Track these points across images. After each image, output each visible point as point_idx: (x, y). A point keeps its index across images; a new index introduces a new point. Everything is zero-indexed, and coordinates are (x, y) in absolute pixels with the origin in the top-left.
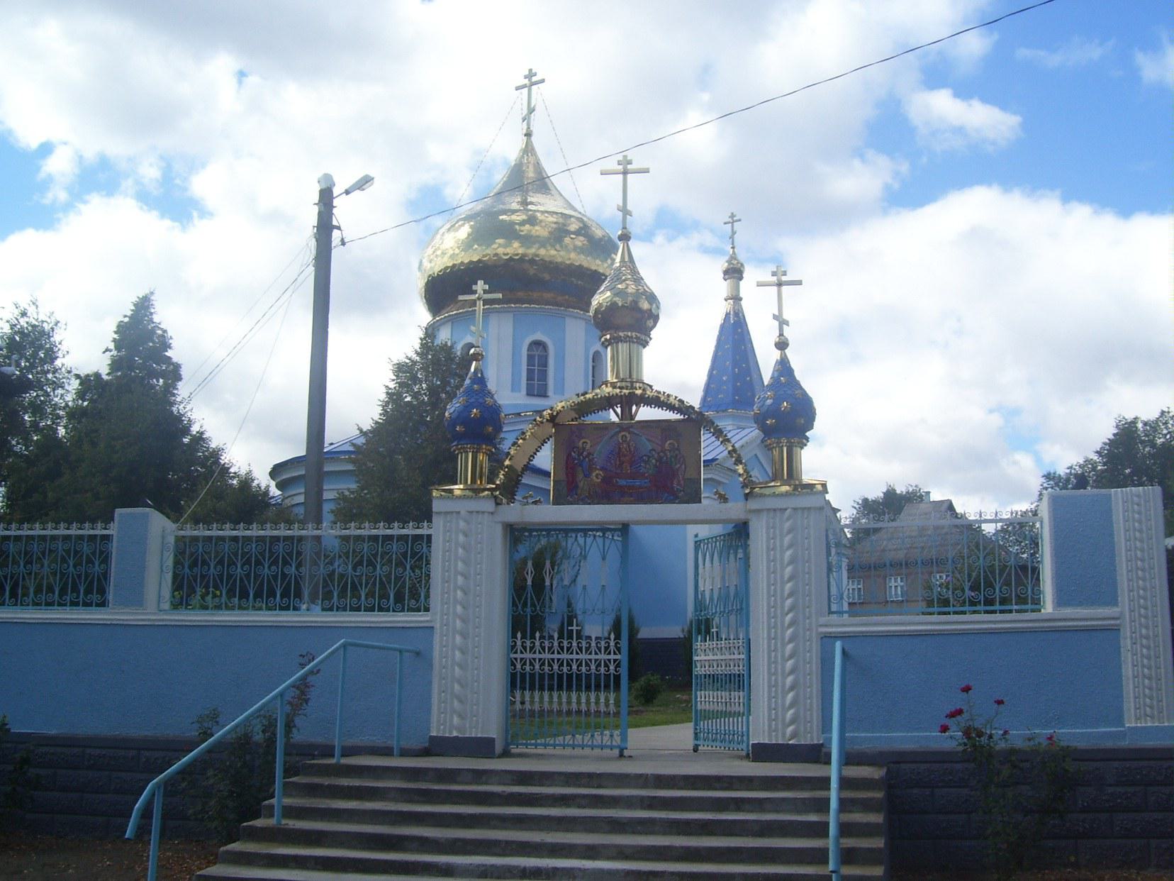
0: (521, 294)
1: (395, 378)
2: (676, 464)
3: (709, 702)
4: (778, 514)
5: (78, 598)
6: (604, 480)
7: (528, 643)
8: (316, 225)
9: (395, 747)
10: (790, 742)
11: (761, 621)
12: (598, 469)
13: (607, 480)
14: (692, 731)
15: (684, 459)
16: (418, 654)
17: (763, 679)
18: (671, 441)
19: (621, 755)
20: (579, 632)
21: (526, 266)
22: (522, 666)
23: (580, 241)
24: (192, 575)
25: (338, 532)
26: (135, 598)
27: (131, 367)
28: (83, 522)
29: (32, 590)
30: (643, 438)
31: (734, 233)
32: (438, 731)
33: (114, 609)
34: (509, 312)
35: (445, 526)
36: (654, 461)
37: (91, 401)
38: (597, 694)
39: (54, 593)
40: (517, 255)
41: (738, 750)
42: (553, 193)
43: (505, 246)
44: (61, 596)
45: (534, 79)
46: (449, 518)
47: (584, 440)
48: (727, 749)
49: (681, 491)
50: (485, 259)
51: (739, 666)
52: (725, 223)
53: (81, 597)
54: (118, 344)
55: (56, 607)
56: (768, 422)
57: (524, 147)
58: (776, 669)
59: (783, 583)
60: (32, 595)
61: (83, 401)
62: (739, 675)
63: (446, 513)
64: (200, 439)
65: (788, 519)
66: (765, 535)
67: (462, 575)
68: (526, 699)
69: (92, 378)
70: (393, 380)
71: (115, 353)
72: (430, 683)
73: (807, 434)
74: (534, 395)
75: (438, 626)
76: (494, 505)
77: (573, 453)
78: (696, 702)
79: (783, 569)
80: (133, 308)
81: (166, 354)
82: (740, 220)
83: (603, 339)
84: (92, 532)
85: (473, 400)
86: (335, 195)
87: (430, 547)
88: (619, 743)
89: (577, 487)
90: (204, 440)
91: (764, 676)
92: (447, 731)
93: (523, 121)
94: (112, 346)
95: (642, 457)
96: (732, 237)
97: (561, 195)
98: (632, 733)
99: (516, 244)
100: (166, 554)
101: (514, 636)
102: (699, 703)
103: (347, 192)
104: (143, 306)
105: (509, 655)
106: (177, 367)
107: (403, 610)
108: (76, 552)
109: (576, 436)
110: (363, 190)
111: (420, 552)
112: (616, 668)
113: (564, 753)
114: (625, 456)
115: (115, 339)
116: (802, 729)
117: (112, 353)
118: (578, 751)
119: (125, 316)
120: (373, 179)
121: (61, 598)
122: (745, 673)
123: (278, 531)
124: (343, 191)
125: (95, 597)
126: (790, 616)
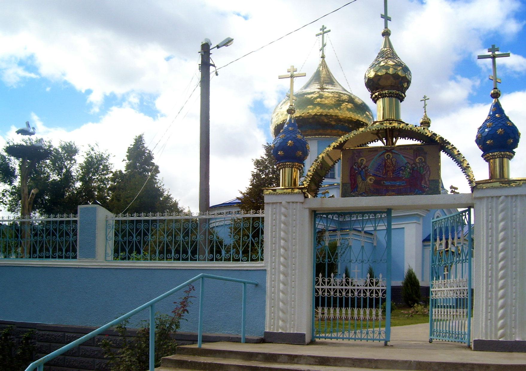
0: (321, 131)
1: (256, 167)
2: (423, 171)
3: (453, 316)
4: (495, 199)
5: (62, 254)
6: (375, 182)
7: (326, 280)
8: (200, 63)
9: (242, 337)
10: (501, 340)
11: (482, 266)
12: (371, 176)
13: (377, 182)
14: (428, 331)
15: (429, 168)
16: (257, 285)
17: (483, 301)
18: (420, 157)
19: (386, 345)
20: (352, 283)
21: (323, 118)
22: (322, 293)
23: (350, 106)
24: (123, 241)
25: (207, 216)
26: (91, 254)
27: (135, 167)
28: (62, 214)
29: (38, 250)
30: (401, 156)
31: (425, 105)
32: (270, 328)
33: (80, 259)
34: (315, 140)
35: (272, 211)
36: (408, 170)
37: (118, 182)
38: (365, 309)
39: (49, 252)
40: (319, 112)
41: (452, 341)
42: (336, 85)
43: (312, 109)
44: (53, 253)
45: (325, 30)
46: (274, 206)
47: (362, 158)
48: (444, 341)
49: (427, 187)
50: (303, 115)
51: (464, 294)
52: (421, 101)
53: (64, 254)
54: (129, 158)
55: (44, 259)
56: (488, 142)
57: (321, 63)
58: (492, 295)
59: (498, 243)
60: (38, 252)
61: (115, 183)
62: (464, 299)
63: (273, 203)
64: (168, 198)
65: (502, 203)
66: (485, 213)
67: (284, 239)
68: (325, 312)
69: (118, 173)
70: (256, 168)
71: (128, 161)
72: (265, 301)
73: (514, 150)
74: (329, 178)
75: (269, 269)
76: (303, 198)
77: (354, 166)
78: (432, 315)
79: (498, 233)
80: (135, 141)
81: (151, 161)
82: (428, 99)
83: (374, 96)
84: (68, 219)
85: (289, 136)
86: (210, 48)
87: (263, 224)
88: (385, 338)
89: (357, 187)
90: (170, 198)
91: (483, 299)
92: (275, 329)
93: (320, 51)
94: (126, 158)
95: (400, 168)
96: (424, 107)
97: (340, 85)
98: (375, 329)
99: (318, 108)
100: (109, 230)
101: (317, 275)
102: (434, 315)
103: (218, 47)
104: (139, 141)
105: (314, 286)
106: (157, 167)
107: (248, 260)
108: (60, 230)
109: (357, 156)
110: (227, 46)
111: (258, 227)
112: (383, 294)
113: (349, 343)
114: (389, 167)
115: (127, 155)
116: (509, 332)
117: (126, 162)
118: (358, 342)
119: (131, 145)
120: (233, 39)
121: (53, 255)
122: (468, 298)
123: (172, 217)
124: (216, 46)
125: (71, 254)
126: (502, 263)
